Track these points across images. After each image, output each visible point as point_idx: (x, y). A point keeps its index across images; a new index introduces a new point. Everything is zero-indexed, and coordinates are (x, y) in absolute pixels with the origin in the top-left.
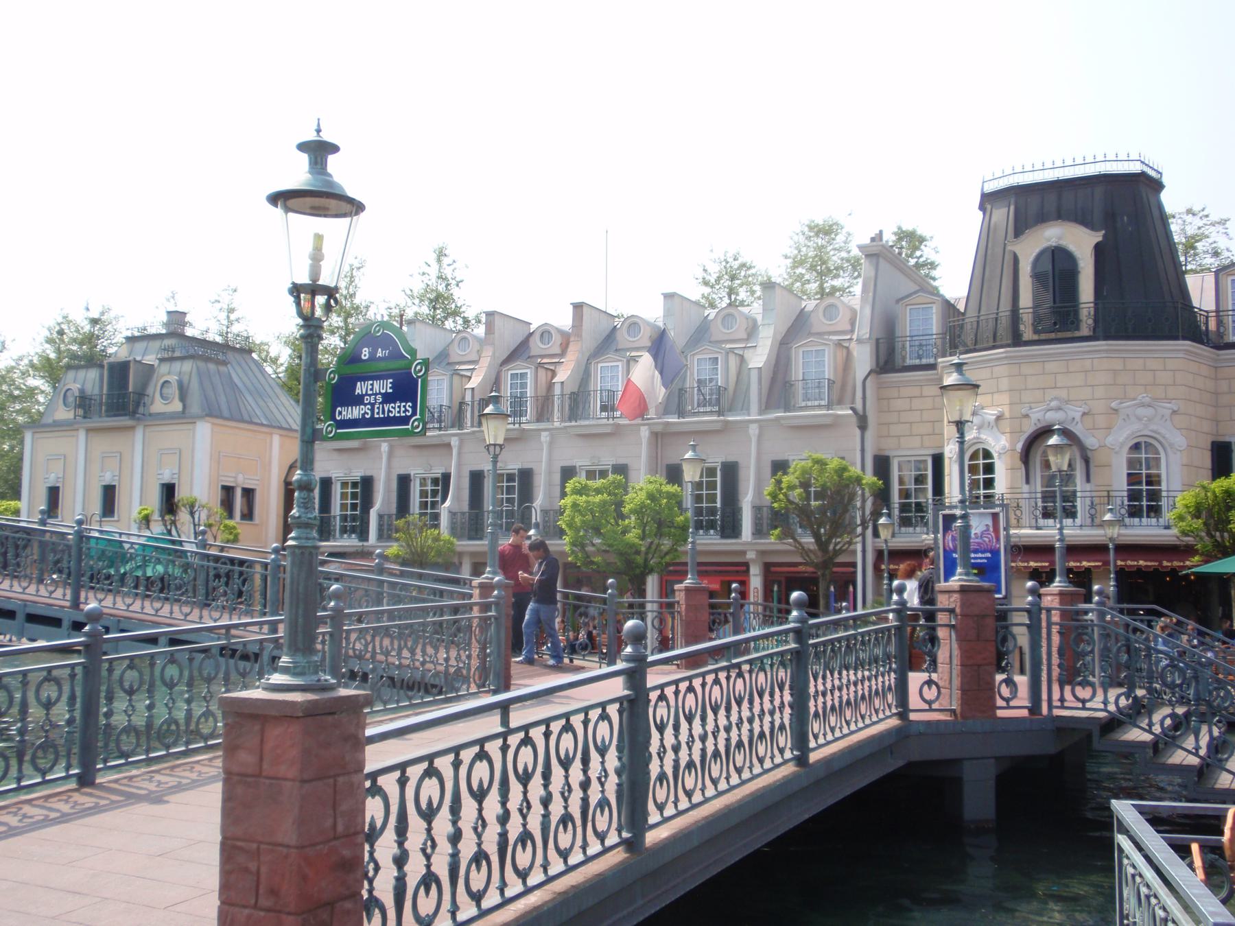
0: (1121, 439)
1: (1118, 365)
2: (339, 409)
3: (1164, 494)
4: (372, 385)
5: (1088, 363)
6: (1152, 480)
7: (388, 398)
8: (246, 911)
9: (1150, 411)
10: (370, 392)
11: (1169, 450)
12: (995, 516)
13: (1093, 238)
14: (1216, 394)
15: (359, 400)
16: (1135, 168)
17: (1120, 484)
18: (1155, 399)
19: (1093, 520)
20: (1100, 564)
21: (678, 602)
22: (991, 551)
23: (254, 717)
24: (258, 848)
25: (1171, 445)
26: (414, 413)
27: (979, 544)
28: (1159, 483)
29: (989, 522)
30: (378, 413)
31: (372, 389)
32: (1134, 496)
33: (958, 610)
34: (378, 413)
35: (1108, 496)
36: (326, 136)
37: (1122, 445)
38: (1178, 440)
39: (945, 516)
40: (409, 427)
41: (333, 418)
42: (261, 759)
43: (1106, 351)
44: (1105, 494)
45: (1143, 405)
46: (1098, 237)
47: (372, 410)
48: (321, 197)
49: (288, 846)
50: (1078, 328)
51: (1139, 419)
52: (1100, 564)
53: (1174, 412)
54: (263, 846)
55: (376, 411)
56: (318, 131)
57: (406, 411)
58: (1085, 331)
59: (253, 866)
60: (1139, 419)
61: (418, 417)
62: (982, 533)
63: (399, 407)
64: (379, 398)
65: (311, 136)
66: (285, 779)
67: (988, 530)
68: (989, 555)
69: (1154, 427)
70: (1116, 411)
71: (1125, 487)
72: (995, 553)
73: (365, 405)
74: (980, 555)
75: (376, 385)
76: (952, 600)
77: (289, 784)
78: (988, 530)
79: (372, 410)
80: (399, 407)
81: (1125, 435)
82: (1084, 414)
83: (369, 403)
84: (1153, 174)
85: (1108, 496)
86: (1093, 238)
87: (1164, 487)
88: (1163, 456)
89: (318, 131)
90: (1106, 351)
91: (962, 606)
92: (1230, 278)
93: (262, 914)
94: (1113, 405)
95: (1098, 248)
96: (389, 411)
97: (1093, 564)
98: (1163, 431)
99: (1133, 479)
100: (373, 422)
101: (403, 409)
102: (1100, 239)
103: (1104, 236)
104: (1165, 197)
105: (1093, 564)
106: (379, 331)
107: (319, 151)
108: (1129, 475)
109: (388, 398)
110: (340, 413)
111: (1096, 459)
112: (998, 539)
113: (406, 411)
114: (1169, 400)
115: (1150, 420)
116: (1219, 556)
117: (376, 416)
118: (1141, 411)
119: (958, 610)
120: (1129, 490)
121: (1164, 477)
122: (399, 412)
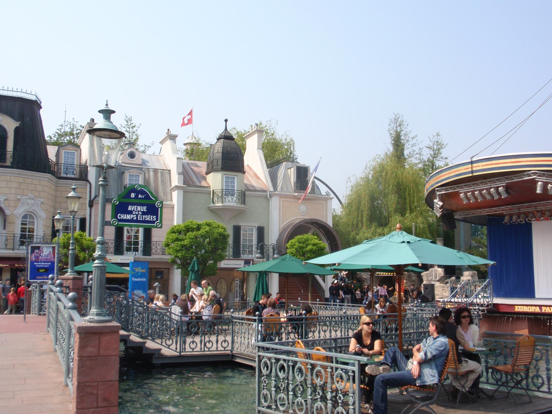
0: (20, 212)
1: (21, 180)
2: (120, 214)
3: (35, 237)
4: (137, 207)
5: (9, 177)
6: (31, 231)
7: (144, 213)
8: (92, 410)
9: (33, 201)
10: (135, 210)
11: (39, 219)
12: (54, 248)
13: (16, 124)
14: (56, 197)
15: (130, 212)
16: (33, 98)
17: (18, 232)
18: (36, 197)
19: (6, 246)
20: (8, 265)
21: (91, 287)
22: (51, 262)
23: (95, 333)
24: (98, 384)
25: (40, 217)
26: (157, 220)
27: (46, 259)
28: (33, 232)
29: (51, 250)
30: (140, 218)
31: (137, 209)
32: (23, 236)
33: (71, 287)
34: (140, 218)
35: (14, 236)
36: (111, 107)
37: (21, 214)
38: (43, 214)
39: (32, 247)
40: (155, 225)
41: (116, 217)
42: (99, 350)
43: (17, 174)
44: (13, 235)
45: (30, 198)
46: (17, 124)
47: (137, 217)
48: (106, 131)
49: (113, 381)
50: (5, 162)
51: (28, 204)
52: (8, 265)
53: (42, 203)
54: (100, 383)
55: (139, 217)
56: (107, 105)
57: (153, 219)
58: (8, 163)
59: (95, 392)
60: (28, 204)
61: (159, 221)
62: (48, 255)
63: (150, 217)
64: (140, 213)
65: (103, 107)
66: (112, 356)
67: (50, 253)
68: (50, 264)
69: (33, 208)
70: (19, 200)
71: (20, 233)
72: (53, 263)
73: (133, 215)
74: (46, 264)
75: (139, 208)
76: (68, 283)
77: (114, 357)
78: (50, 253)
79: (137, 217)
80: (150, 217)
81: (22, 211)
82: (5, 200)
83: (135, 214)
84: (39, 102)
85: (14, 236)
86: (16, 124)
87: (35, 234)
88: (36, 220)
89: (107, 105)
90: (17, 174)
91: (73, 285)
92: (64, 151)
93: (101, 409)
94: (18, 197)
95: (17, 130)
96: (145, 218)
97: (5, 265)
98: (37, 210)
99: (23, 230)
100: (137, 221)
101: (152, 218)
102: (18, 125)
103: (20, 124)
104: (41, 111)
105: (5, 265)
106: (139, 188)
107: (107, 113)
108: (22, 228)
109: (144, 213)
110: (120, 216)
111: (9, 220)
112: (54, 257)
113: (153, 219)
114: (41, 198)
115: (32, 205)
116: (366, 276)
117: (139, 219)
118: (30, 201)
119: (71, 287)
120: (21, 234)
121: (35, 230)
122: (150, 219)
